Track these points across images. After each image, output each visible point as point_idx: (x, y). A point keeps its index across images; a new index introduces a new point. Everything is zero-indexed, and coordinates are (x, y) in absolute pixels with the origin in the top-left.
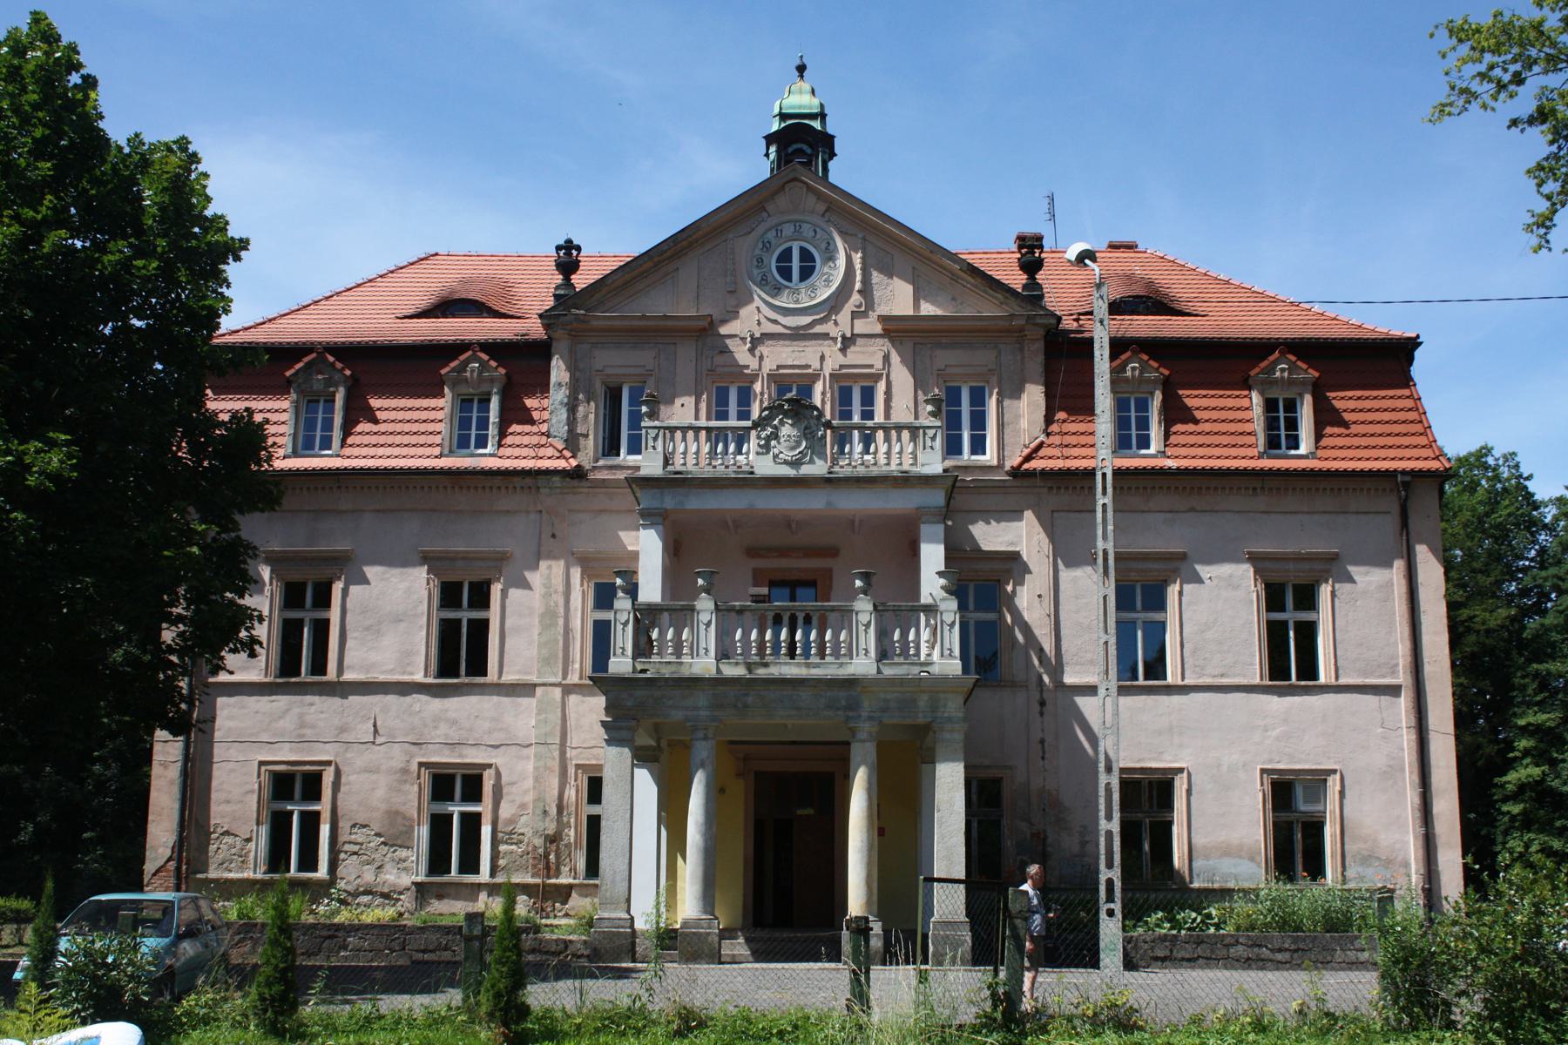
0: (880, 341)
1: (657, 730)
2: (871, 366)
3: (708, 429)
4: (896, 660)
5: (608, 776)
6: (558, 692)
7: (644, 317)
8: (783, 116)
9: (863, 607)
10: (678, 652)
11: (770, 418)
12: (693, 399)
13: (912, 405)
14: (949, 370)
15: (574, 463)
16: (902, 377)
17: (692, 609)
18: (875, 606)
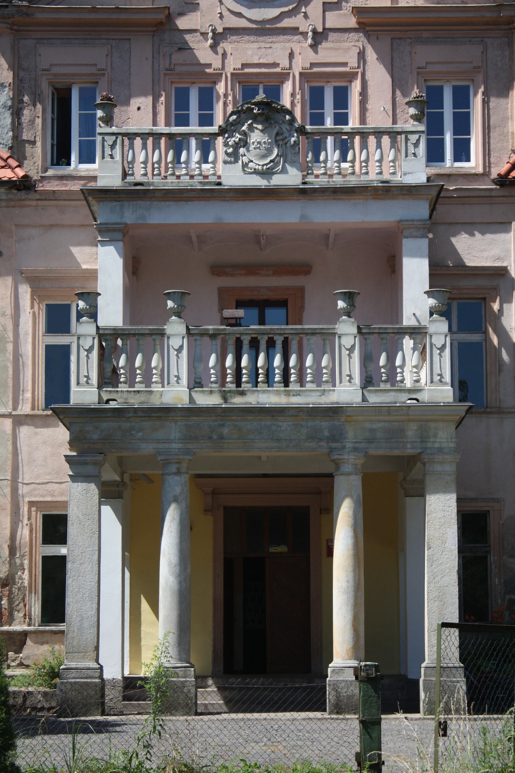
0: (353, 36)
1: (121, 464)
2: (345, 64)
3: (170, 136)
4: (382, 386)
5: (74, 514)
6: (8, 423)
7: (94, 10)
9: (347, 329)
10: (147, 381)
11: (238, 123)
12: (150, 99)
13: (389, 107)
14: (430, 68)
15: (20, 172)
16: (378, 76)
17: (162, 334)
18: (359, 328)
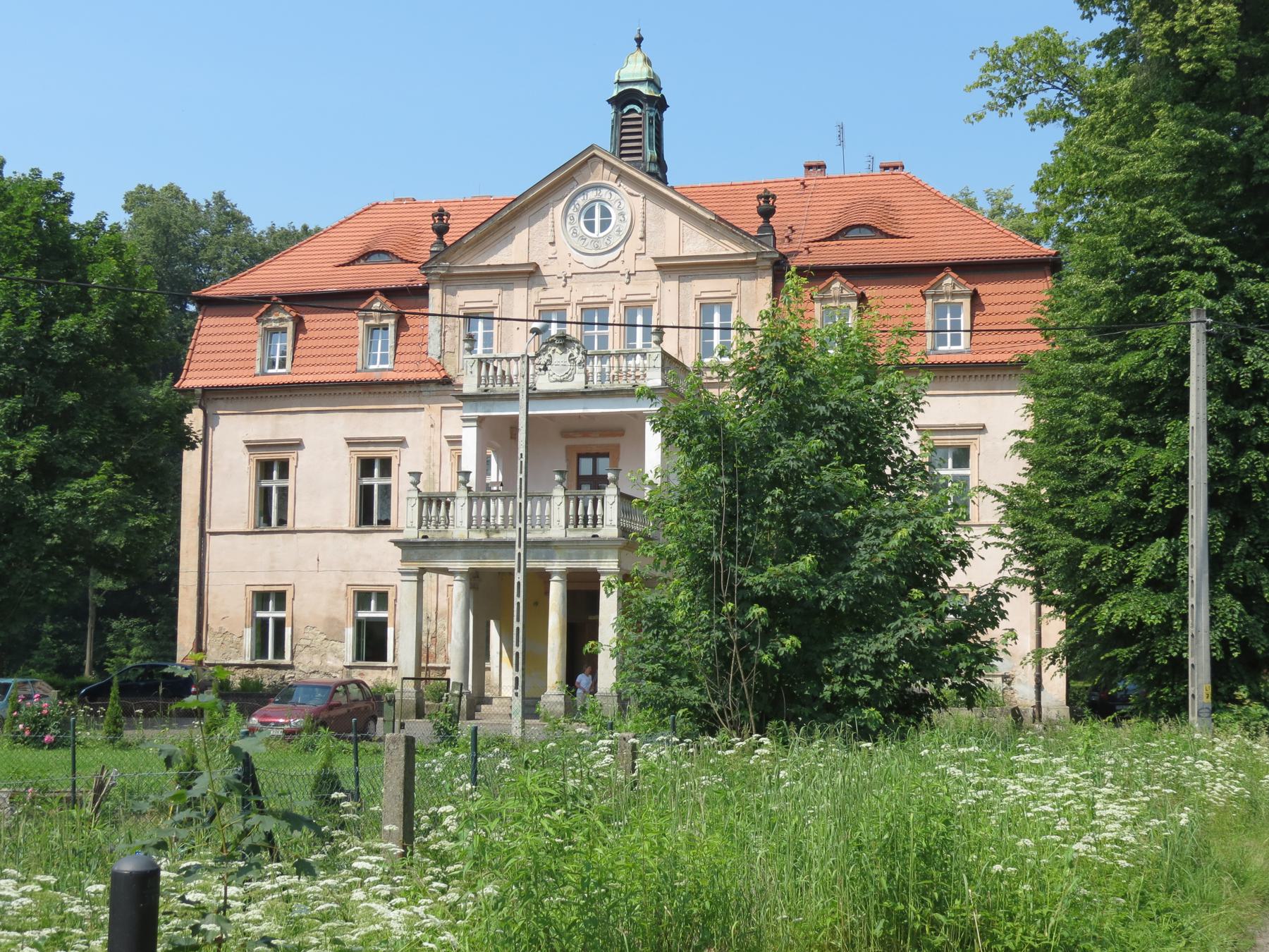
8: (619, 83)
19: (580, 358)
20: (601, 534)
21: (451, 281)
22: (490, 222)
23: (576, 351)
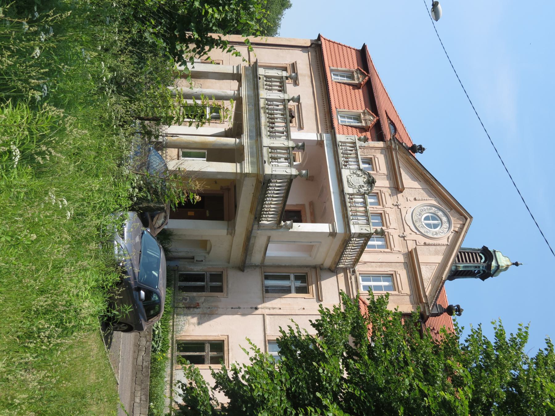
7: (399, 167)
8: (495, 251)
13: (380, 261)
19: (362, 190)
20: (266, 165)
21: (388, 151)
22: (422, 169)
23: (366, 189)
